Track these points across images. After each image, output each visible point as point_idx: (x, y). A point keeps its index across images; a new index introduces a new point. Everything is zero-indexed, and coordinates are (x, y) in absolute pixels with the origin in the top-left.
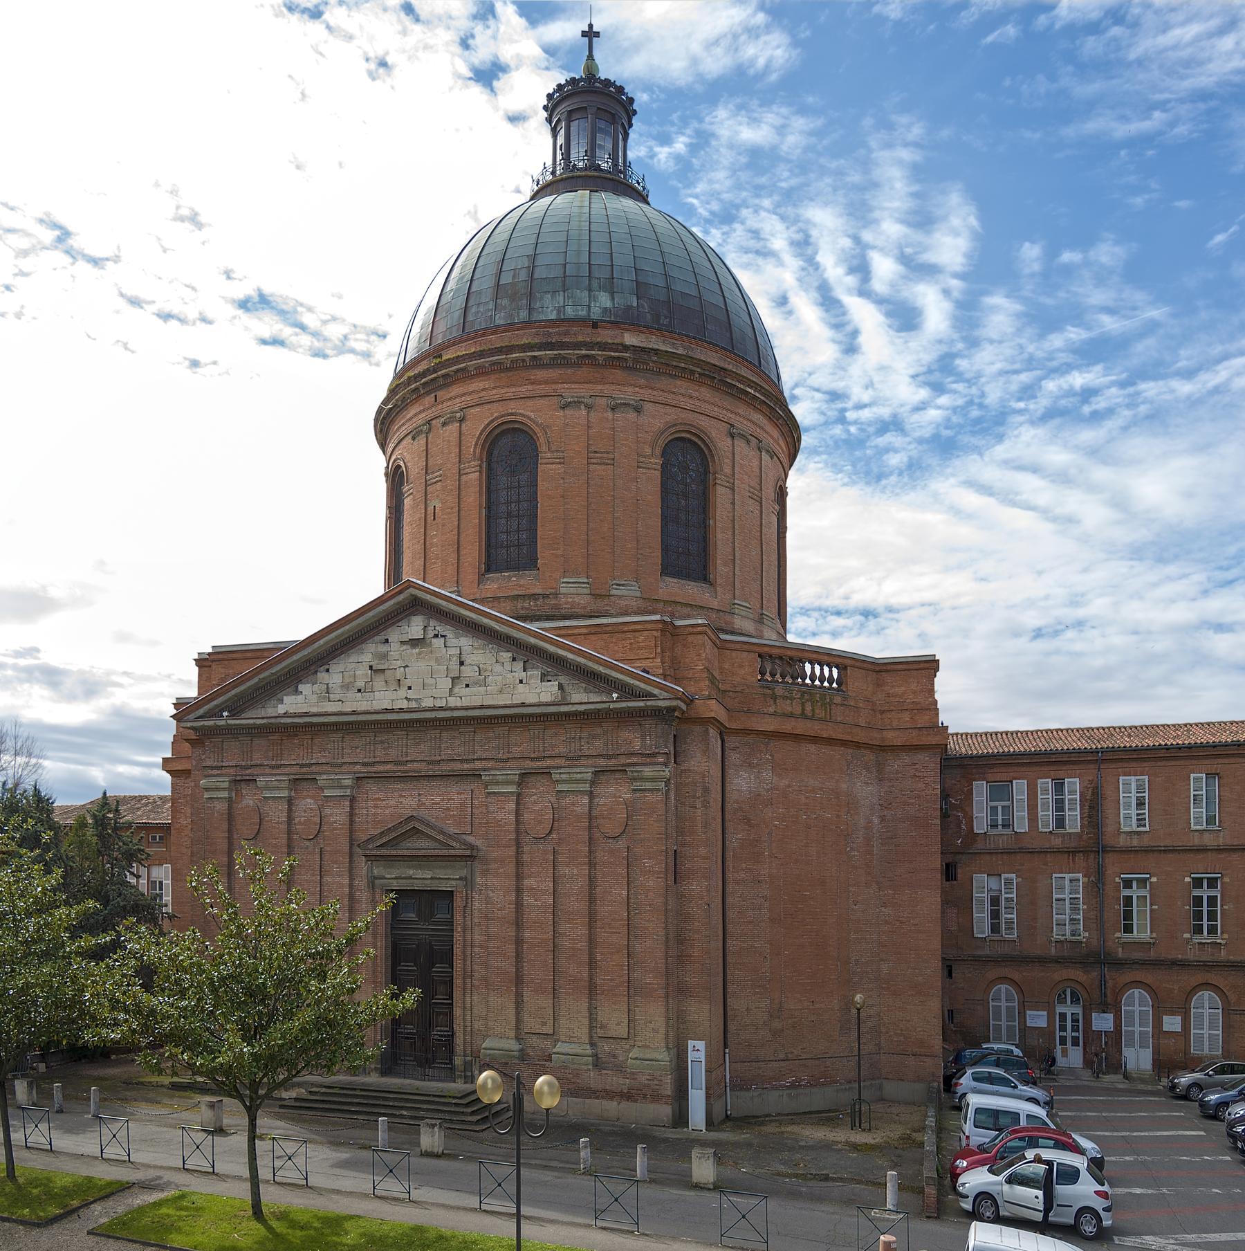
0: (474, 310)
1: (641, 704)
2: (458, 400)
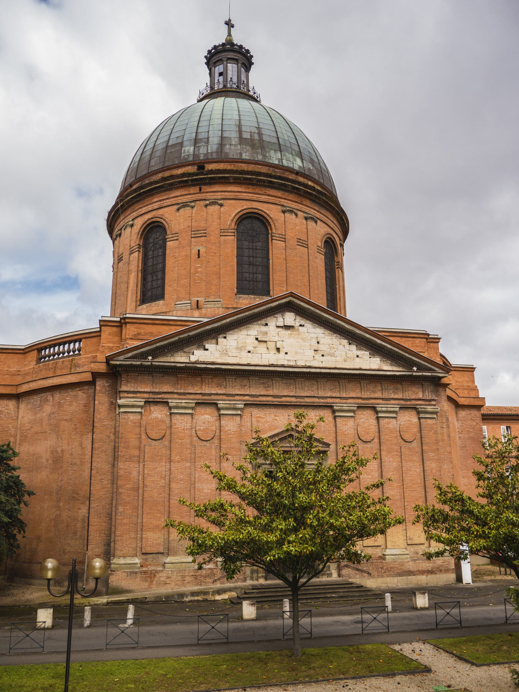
1: (430, 374)
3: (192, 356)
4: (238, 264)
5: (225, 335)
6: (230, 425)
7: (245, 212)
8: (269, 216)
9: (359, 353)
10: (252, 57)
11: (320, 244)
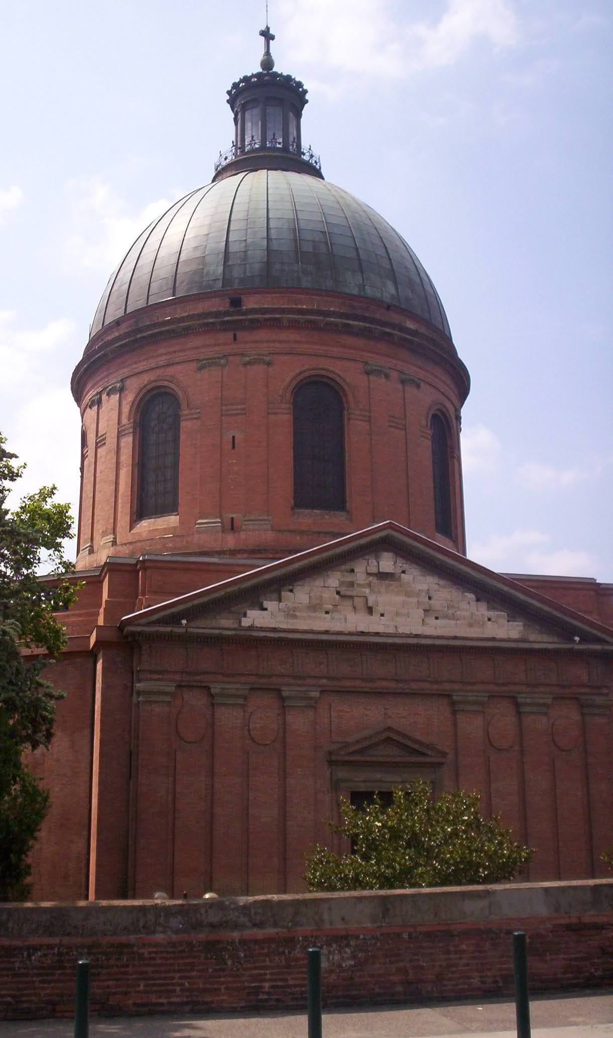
0: (277, 266)
2: (265, 345)
3: (243, 619)
4: (295, 458)
5: (291, 587)
6: (299, 722)
7: (307, 374)
8: (344, 381)
9: (491, 614)
10: (305, 92)
11: (424, 423)
